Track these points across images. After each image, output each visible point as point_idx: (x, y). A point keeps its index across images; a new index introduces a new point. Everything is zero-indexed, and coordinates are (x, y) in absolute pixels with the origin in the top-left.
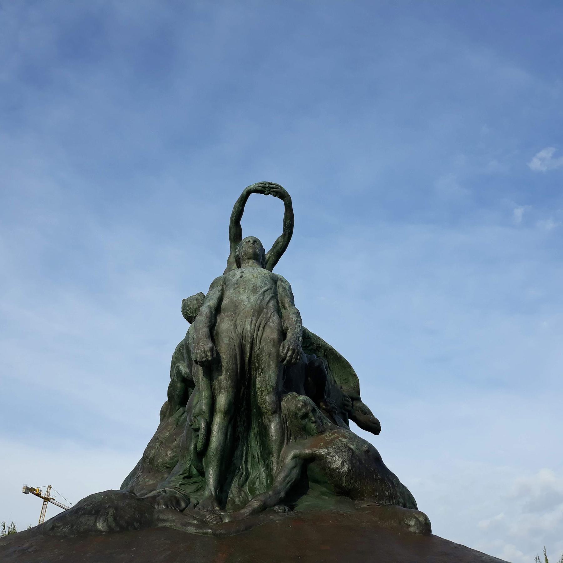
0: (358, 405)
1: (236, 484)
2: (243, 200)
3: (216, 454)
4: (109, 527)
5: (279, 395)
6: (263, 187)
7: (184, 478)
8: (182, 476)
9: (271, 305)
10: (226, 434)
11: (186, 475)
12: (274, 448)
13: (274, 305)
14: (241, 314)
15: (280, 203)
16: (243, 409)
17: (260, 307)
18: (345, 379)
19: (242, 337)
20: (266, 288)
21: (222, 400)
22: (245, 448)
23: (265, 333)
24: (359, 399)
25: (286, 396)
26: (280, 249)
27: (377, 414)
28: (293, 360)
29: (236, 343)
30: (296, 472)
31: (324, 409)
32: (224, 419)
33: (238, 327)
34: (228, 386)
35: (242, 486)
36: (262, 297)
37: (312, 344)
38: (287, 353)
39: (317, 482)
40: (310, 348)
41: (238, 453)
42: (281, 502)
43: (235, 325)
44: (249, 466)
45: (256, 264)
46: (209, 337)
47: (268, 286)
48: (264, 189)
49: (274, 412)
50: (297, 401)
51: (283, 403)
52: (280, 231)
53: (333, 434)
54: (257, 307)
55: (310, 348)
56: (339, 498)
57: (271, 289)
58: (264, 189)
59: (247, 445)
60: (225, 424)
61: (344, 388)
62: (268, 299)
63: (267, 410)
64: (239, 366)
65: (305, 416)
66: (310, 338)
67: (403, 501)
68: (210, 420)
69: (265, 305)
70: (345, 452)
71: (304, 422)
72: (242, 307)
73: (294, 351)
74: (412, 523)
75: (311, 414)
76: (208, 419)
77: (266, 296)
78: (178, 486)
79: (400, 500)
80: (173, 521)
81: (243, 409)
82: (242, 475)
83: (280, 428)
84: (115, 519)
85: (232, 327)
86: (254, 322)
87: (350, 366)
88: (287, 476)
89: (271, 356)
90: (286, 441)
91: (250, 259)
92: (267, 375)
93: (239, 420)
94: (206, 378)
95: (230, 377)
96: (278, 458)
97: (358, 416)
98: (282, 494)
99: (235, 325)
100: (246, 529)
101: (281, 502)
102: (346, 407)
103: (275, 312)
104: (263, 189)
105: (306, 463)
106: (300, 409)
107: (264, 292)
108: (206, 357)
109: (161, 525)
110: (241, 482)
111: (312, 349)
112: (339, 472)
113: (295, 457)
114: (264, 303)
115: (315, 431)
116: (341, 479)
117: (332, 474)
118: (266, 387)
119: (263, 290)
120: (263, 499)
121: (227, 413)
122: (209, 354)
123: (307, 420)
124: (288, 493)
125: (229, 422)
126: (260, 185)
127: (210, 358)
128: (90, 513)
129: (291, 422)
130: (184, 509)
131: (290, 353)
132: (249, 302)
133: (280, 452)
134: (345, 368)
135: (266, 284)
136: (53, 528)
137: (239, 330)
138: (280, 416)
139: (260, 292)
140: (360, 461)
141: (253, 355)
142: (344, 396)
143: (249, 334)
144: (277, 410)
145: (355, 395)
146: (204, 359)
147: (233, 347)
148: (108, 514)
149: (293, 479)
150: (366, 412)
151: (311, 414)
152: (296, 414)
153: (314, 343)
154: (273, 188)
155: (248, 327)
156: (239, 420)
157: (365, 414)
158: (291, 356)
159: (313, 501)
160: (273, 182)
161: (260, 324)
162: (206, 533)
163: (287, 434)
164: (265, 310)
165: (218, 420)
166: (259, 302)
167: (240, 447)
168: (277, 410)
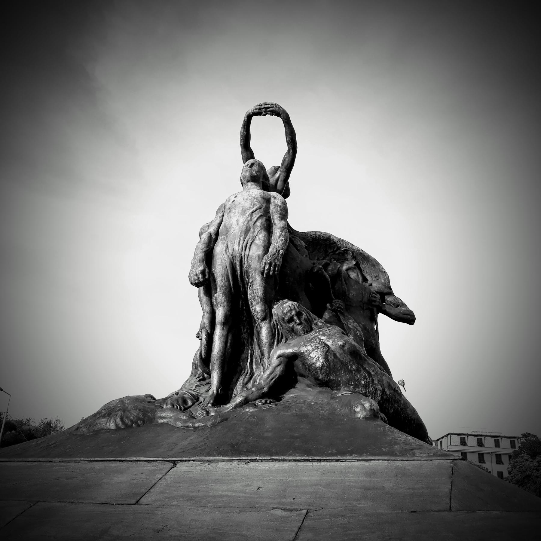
0: (389, 299)
1: (241, 383)
2: (249, 118)
3: (218, 359)
4: (117, 425)
5: (269, 302)
6: (260, 109)
7: (200, 381)
8: (198, 379)
9: (258, 224)
10: (226, 342)
11: (201, 378)
12: (265, 349)
13: (261, 223)
14: (231, 236)
15: (279, 121)
16: (244, 319)
17: (247, 228)
18: (376, 276)
19: (233, 257)
20: (254, 209)
21: (220, 314)
22: (250, 351)
23: (251, 251)
24: (391, 294)
25: (277, 304)
26: (288, 166)
27: (411, 306)
28: (271, 273)
29: (228, 263)
30: (279, 370)
31: (330, 309)
32: (223, 329)
33: (230, 248)
34: (223, 301)
35: (247, 383)
36: (249, 218)
37: (339, 248)
38: (265, 267)
39: (302, 376)
40: (337, 252)
41: (244, 356)
42: (263, 396)
43: (227, 247)
44: (254, 366)
45: (254, 186)
46: (203, 261)
47: (257, 206)
48: (263, 111)
49: (264, 319)
50: (284, 307)
51: (274, 311)
52: (284, 148)
53: (315, 333)
54: (244, 228)
55: (337, 252)
56: (321, 389)
57: (261, 208)
58: (263, 111)
59: (252, 348)
60: (225, 333)
61: (374, 285)
62: (256, 219)
63: (257, 318)
64: (231, 283)
65: (291, 320)
66: (335, 243)
67: (381, 388)
68: (211, 331)
69: (251, 225)
70: (321, 348)
71: (291, 325)
72: (232, 230)
73: (270, 264)
74: (358, 410)
75: (295, 318)
76: (209, 331)
77: (254, 216)
78: (194, 388)
79: (377, 387)
80: (171, 418)
81: (244, 319)
82: (247, 374)
83: (269, 333)
84: (122, 419)
85: (224, 250)
86: (241, 242)
87: (378, 264)
88: (271, 374)
89: (257, 271)
90: (276, 343)
91: (248, 182)
92: (254, 288)
93: (242, 328)
94: (206, 296)
95: (224, 293)
96: (268, 358)
97: (387, 310)
98: (265, 390)
99: (227, 247)
100: (222, 421)
101: (263, 396)
102: (373, 303)
103: (262, 230)
104: (260, 111)
105: (291, 361)
106: (286, 314)
107: (253, 212)
108: (198, 279)
109: (161, 421)
110: (246, 380)
111: (339, 253)
112: (315, 367)
113: (279, 357)
114: (251, 223)
115: (301, 332)
116: (317, 373)
117: (310, 368)
118: (254, 299)
119: (251, 211)
120: (245, 395)
121: (224, 324)
122: (200, 276)
123: (293, 323)
124: (271, 388)
125: (228, 332)
126: (257, 107)
127: (201, 280)
128: (104, 416)
129: (282, 326)
130: (190, 407)
131: (267, 267)
132: (238, 224)
133: (270, 352)
134: (374, 266)
135: (255, 205)
136: (77, 429)
137: (230, 251)
138: (270, 321)
139: (248, 214)
140: (335, 355)
141: (244, 271)
142: (371, 293)
143: (238, 254)
144: (268, 315)
145: (386, 290)
146: (197, 281)
147: (225, 267)
148: (116, 416)
149: (276, 375)
150: (399, 304)
151: (295, 318)
152: (283, 319)
153: (340, 247)
154: (268, 108)
155: (236, 248)
156: (242, 328)
157: (398, 306)
158: (269, 269)
159: (302, 394)
160: (268, 102)
161: (247, 243)
162: (188, 427)
163: (278, 337)
164: (252, 230)
165: (218, 332)
166: (246, 223)
167: (245, 351)
168: (268, 315)
